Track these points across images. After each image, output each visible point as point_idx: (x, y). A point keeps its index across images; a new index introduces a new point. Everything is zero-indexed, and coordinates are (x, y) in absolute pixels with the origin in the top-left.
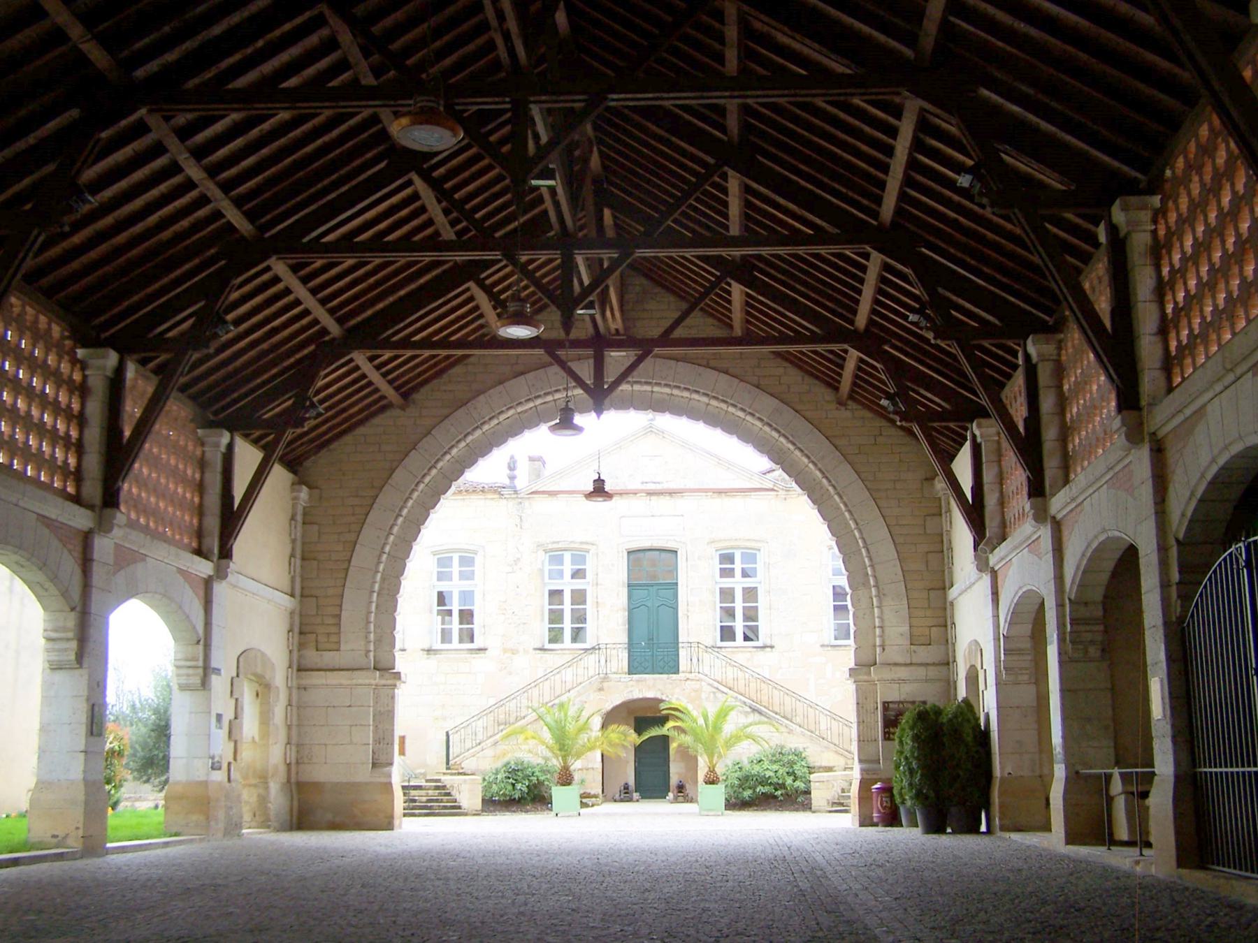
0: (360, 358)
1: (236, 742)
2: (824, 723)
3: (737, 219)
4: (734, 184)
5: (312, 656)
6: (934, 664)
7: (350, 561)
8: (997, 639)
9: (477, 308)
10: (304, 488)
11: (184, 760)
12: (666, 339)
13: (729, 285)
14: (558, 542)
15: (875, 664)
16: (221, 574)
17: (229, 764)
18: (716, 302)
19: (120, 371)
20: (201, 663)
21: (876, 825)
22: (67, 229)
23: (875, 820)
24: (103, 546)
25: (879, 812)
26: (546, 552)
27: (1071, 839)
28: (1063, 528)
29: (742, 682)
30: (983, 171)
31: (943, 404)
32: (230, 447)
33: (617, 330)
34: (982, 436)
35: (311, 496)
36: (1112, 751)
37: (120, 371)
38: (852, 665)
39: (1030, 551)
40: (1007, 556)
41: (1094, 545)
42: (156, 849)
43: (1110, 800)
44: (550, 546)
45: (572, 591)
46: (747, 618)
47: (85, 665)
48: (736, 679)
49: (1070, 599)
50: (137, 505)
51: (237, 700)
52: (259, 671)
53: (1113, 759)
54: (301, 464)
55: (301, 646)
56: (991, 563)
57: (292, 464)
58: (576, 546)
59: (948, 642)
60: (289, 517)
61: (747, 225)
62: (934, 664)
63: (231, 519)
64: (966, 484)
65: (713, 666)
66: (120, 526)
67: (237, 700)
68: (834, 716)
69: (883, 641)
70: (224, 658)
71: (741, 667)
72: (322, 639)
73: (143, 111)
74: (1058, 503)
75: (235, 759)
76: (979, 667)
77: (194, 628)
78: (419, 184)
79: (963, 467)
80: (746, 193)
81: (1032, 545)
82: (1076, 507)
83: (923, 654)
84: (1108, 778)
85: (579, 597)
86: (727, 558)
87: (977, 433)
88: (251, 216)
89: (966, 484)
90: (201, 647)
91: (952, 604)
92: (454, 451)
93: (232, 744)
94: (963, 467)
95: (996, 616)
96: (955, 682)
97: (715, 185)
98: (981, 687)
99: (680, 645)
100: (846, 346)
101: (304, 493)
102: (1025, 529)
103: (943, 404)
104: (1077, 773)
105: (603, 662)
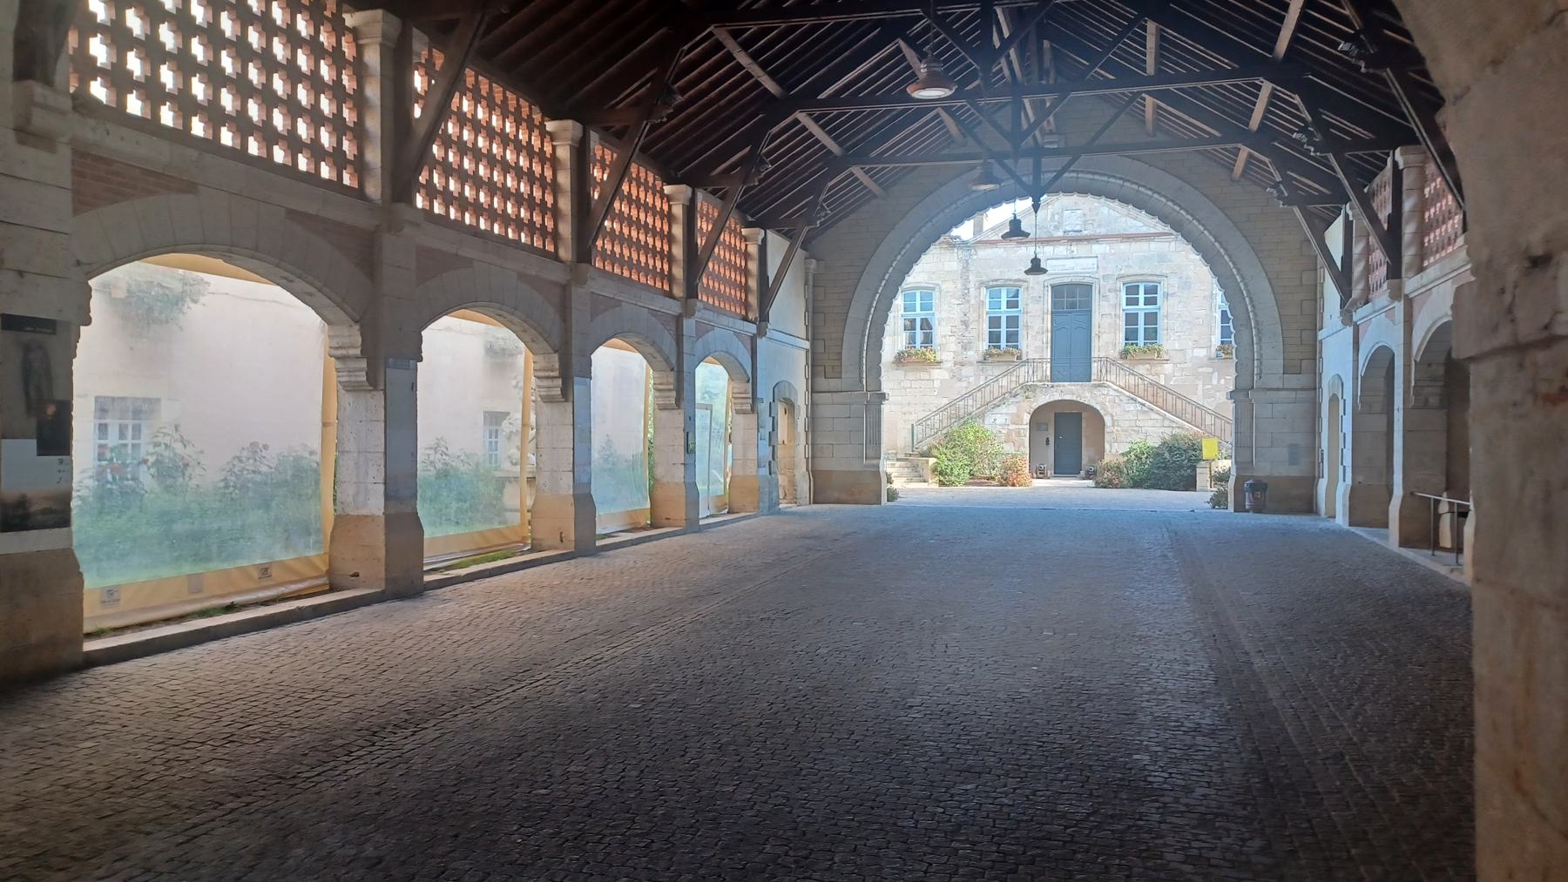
0: (856, 170)
1: (774, 447)
2: (1209, 420)
3: (1153, 50)
4: (1152, 26)
5: (823, 383)
6: (1302, 389)
7: (847, 313)
8: (1355, 378)
9: (941, 122)
10: (813, 260)
11: (741, 461)
12: (1089, 149)
13: (1144, 99)
14: (997, 280)
15: (1253, 387)
16: (761, 332)
17: (770, 463)
18: (1125, 51)
19: (693, 200)
20: (750, 395)
21: (1247, 511)
22: (665, 119)
23: (1247, 507)
24: (689, 325)
25: (1251, 502)
26: (987, 288)
27: (1405, 542)
28: (1414, 305)
29: (1141, 387)
30: (1362, 36)
31: (1321, 189)
32: (764, 240)
33: (1051, 131)
34: (1353, 216)
35: (818, 265)
36: (1444, 478)
37: (693, 200)
38: (1232, 388)
39: (1386, 316)
40: (1367, 316)
41: (1439, 324)
42: (727, 524)
43: (1438, 517)
44: (991, 283)
45: (1007, 317)
46: (1148, 302)
47: (682, 406)
48: (1137, 386)
49: (1415, 361)
50: (711, 292)
51: (774, 418)
52: (787, 396)
53: (1443, 485)
54: (810, 243)
55: (813, 375)
56: (1354, 319)
57: (804, 246)
58: (1012, 283)
59: (1315, 373)
60: (803, 283)
61: (1161, 45)
62: (1302, 389)
63: (767, 293)
64: (1337, 253)
65: (1117, 379)
66: (699, 311)
67: (774, 418)
68: (1217, 416)
69: (1261, 370)
70: (764, 392)
71: (1142, 377)
72: (829, 370)
73: (711, 28)
74: (1411, 284)
75: (773, 459)
76: (1340, 397)
77: (746, 372)
78: (902, 44)
79: (1335, 236)
80: (1161, 49)
81: (1390, 313)
82: (1426, 291)
83: (1294, 381)
84: (1437, 502)
85: (1013, 321)
86: (1132, 290)
87: (1350, 213)
88: (780, 82)
89: (1337, 253)
90: (750, 384)
91: (1321, 342)
92: (923, 230)
93: (771, 448)
94: (1335, 236)
95: (1356, 361)
96: (1320, 404)
97: (1138, 102)
98: (1341, 413)
99: (1093, 359)
100: (1239, 145)
101: (813, 264)
102: (1381, 298)
103: (1321, 189)
104: (1412, 493)
105: (1031, 372)
